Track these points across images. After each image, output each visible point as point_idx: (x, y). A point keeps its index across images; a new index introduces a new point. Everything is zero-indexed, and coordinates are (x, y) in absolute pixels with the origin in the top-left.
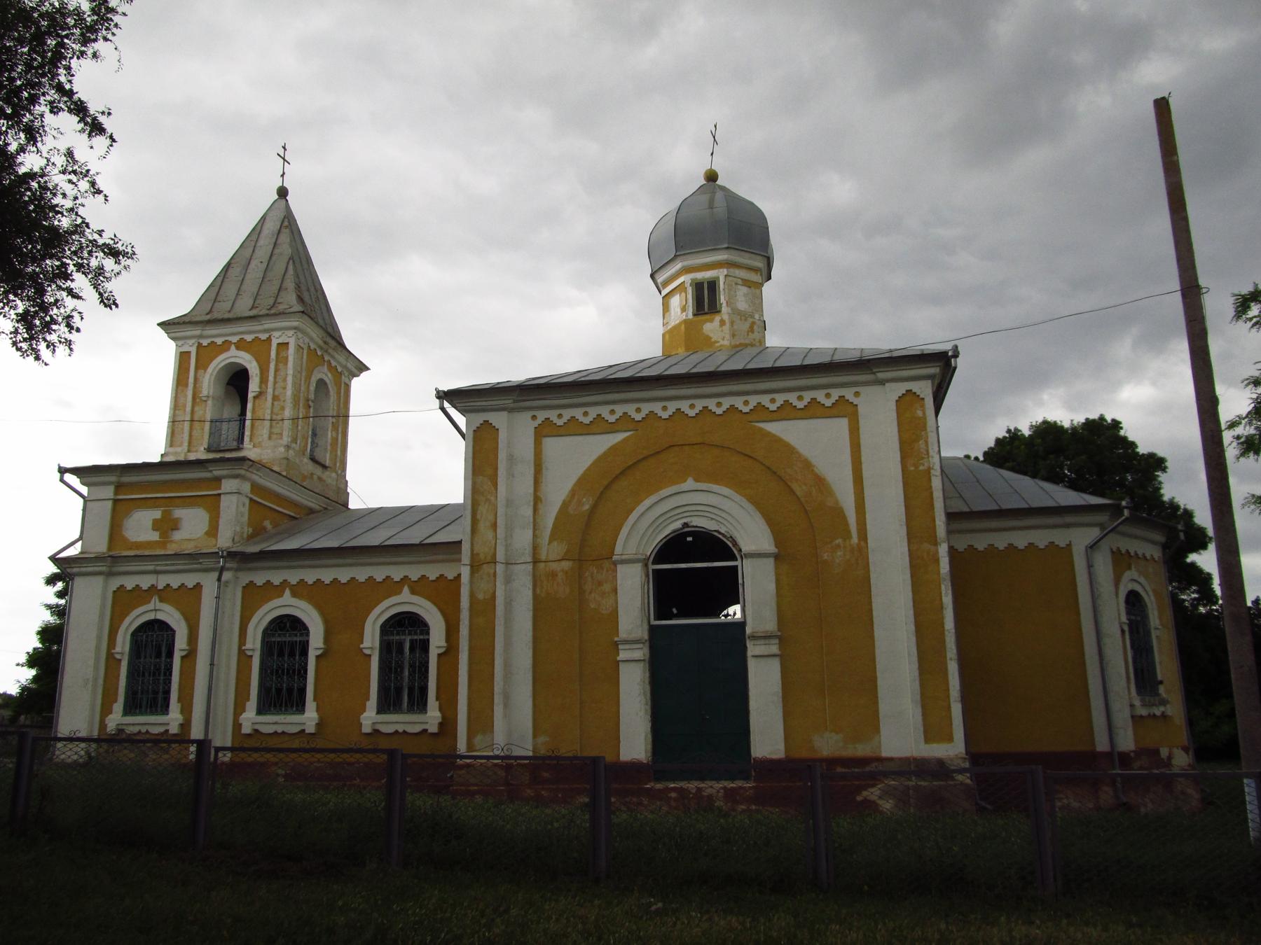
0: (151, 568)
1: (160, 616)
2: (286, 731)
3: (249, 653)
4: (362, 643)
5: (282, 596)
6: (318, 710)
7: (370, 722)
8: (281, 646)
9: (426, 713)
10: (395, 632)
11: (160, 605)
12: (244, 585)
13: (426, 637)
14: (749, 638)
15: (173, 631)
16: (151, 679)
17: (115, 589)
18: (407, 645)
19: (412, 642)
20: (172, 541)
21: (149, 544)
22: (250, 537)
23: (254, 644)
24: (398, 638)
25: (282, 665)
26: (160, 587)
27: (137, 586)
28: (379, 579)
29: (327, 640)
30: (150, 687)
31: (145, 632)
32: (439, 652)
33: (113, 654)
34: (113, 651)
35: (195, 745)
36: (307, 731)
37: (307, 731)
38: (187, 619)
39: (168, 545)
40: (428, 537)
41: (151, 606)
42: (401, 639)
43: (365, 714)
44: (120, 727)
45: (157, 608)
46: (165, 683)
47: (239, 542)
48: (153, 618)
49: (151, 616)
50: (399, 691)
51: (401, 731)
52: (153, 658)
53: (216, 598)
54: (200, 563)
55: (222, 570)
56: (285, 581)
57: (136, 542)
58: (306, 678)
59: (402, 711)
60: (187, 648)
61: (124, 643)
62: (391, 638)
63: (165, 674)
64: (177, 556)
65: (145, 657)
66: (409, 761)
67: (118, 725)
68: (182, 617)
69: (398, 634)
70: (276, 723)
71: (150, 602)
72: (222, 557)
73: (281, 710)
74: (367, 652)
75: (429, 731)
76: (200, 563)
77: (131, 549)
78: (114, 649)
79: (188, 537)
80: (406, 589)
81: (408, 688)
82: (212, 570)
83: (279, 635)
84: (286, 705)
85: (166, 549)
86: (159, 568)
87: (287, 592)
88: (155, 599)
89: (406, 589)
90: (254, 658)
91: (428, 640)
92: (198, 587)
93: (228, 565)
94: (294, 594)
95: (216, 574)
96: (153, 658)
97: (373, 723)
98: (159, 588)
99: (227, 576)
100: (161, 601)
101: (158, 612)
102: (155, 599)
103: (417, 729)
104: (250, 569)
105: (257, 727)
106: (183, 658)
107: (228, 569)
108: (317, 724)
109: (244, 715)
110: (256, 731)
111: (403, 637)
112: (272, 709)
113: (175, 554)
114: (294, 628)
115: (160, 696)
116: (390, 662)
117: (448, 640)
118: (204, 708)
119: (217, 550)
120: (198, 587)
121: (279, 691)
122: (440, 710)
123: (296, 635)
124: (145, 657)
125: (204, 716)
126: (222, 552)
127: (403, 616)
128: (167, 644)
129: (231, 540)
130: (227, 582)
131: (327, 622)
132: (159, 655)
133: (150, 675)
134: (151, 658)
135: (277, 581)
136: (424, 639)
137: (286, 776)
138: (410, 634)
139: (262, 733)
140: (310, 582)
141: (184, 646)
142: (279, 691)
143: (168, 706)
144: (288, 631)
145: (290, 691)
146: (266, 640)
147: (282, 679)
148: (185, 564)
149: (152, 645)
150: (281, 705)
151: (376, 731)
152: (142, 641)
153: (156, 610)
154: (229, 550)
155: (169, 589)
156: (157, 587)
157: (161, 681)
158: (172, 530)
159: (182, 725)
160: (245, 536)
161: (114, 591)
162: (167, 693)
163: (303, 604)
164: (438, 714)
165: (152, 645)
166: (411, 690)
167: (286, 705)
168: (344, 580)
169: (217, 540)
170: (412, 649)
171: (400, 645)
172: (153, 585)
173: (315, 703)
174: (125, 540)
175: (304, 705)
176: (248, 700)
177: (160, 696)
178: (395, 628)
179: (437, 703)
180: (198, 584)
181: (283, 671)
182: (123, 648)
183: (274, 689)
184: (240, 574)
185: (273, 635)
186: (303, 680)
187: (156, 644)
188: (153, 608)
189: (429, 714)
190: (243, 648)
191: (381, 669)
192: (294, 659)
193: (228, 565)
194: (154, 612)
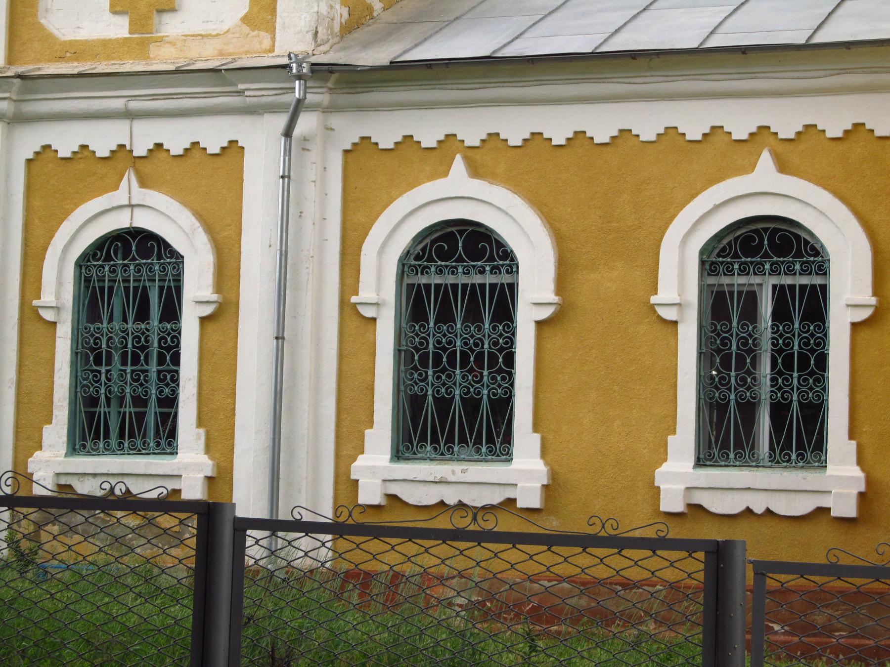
0: (117, 104)
1: (144, 221)
2: (465, 501)
3: (368, 312)
4: (655, 291)
5: (446, 174)
6: (544, 452)
7: (682, 487)
8: (445, 294)
9: (510, 460)
10: (736, 266)
11: (141, 195)
12: (349, 147)
13: (818, 280)
14: (52, 293)
15: (178, 258)
16: (129, 369)
17: (31, 156)
18: (766, 306)
19: (781, 295)
20: (160, 40)
21: (107, 47)
22: (348, 29)
23: (378, 290)
24: (742, 280)
25: (450, 343)
26: (140, 150)
27: (84, 147)
28: (694, 134)
29: (561, 283)
30: (128, 390)
31: (108, 258)
32: (204, 315)
33: (35, 310)
34: (35, 303)
35: (701, 555)
36: (520, 504)
37: (520, 504)
38: (210, 229)
39: (153, 49)
40: (613, 35)
41: (120, 196)
42: (751, 285)
43: (665, 468)
44: (63, 481)
45: (134, 202)
46: (159, 379)
47: (328, 41)
48: (128, 225)
49: (121, 221)
50: (749, 410)
51: (759, 509)
52: (131, 318)
53: (282, 177)
54: (240, 93)
55: (299, 107)
56: (450, 137)
57: (71, 41)
58: (511, 375)
59: (757, 460)
60: (215, 297)
61: (60, 283)
62: (725, 280)
63: (161, 360)
64: (180, 73)
65: (111, 320)
66: (771, 583)
67: (58, 475)
68: (198, 224)
69: (743, 271)
70: (442, 482)
71: (116, 187)
72: (299, 77)
73: (478, 451)
74: (669, 314)
75: (834, 513)
76: (240, 93)
77: (61, 58)
78: (357, 294)
79: (199, 29)
80: (766, 160)
81: (772, 405)
82: (273, 109)
83: (440, 272)
84: (800, 446)
85: (148, 58)
86: (135, 105)
87: (458, 165)
88: (130, 179)
89: (766, 160)
90: (681, 328)
91: (824, 288)
92: (233, 149)
93: (311, 98)
94: (475, 171)
95: (281, 121)
96: (131, 318)
97: (688, 488)
98: (136, 153)
99: (306, 123)
100: (143, 184)
101: (137, 211)
102: (130, 179)
103: (802, 506)
104: (361, 108)
105: (394, 489)
106: (540, 324)
107: (314, 107)
108: (862, 495)
109: (361, 461)
110: (393, 498)
111: (756, 280)
112: (429, 448)
113: (178, 71)
114: (474, 253)
115: (152, 410)
116: (725, 342)
117: (218, 287)
118: (265, 438)
119: (285, 61)
120: (233, 149)
121: (443, 404)
122: (860, 461)
123: (482, 272)
124: (111, 320)
125: (265, 458)
126: (300, 65)
127: (760, 226)
128: (161, 288)
129: (310, 36)
130: (305, 139)
131: (560, 239)
132: (143, 314)
133: (124, 363)
134: (125, 320)
135: (429, 140)
136: (813, 287)
137: (470, 607)
138: (774, 272)
139: (406, 504)
140: (515, 140)
141: (207, 293)
142: (443, 404)
143: (172, 434)
144: (460, 260)
145: (471, 405)
146: (407, 281)
147: (449, 376)
148: (206, 95)
149: (127, 289)
150: (478, 441)
151: (696, 509)
152: (101, 280)
153: (131, 206)
154: (313, 60)
155: (162, 155)
156: (131, 151)
157: (153, 376)
158: (160, 11)
159: (210, 480)
160: (337, 28)
161: (29, 161)
162: (170, 402)
163: (499, 194)
164: (857, 472)
165: (127, 289)
166: (779, 412)
167: (490, 440)
168: (602, 136)
169: (273, 39)
170: (781, 314)
171: (751, 299)
172: (122, 147)
173: (537, 437)
174: (48, 38)
175: (508, 439)
176: (370, 423)
177: (152, 410)
178: (736, 256)
179: (202, 431)
180: (233, 143)
181: (480, 357)
182: (58, 296)
183: (430, 398)
184: (337, 121)
185: (425, 270)
186: (503, 379)
187: (136, 289)
188: (127, 203)
189: (833, 469)
190: (354, 299)
191: (705, 357)
192: (479, 329)
193: (311, 98)
194: (128, 211)
